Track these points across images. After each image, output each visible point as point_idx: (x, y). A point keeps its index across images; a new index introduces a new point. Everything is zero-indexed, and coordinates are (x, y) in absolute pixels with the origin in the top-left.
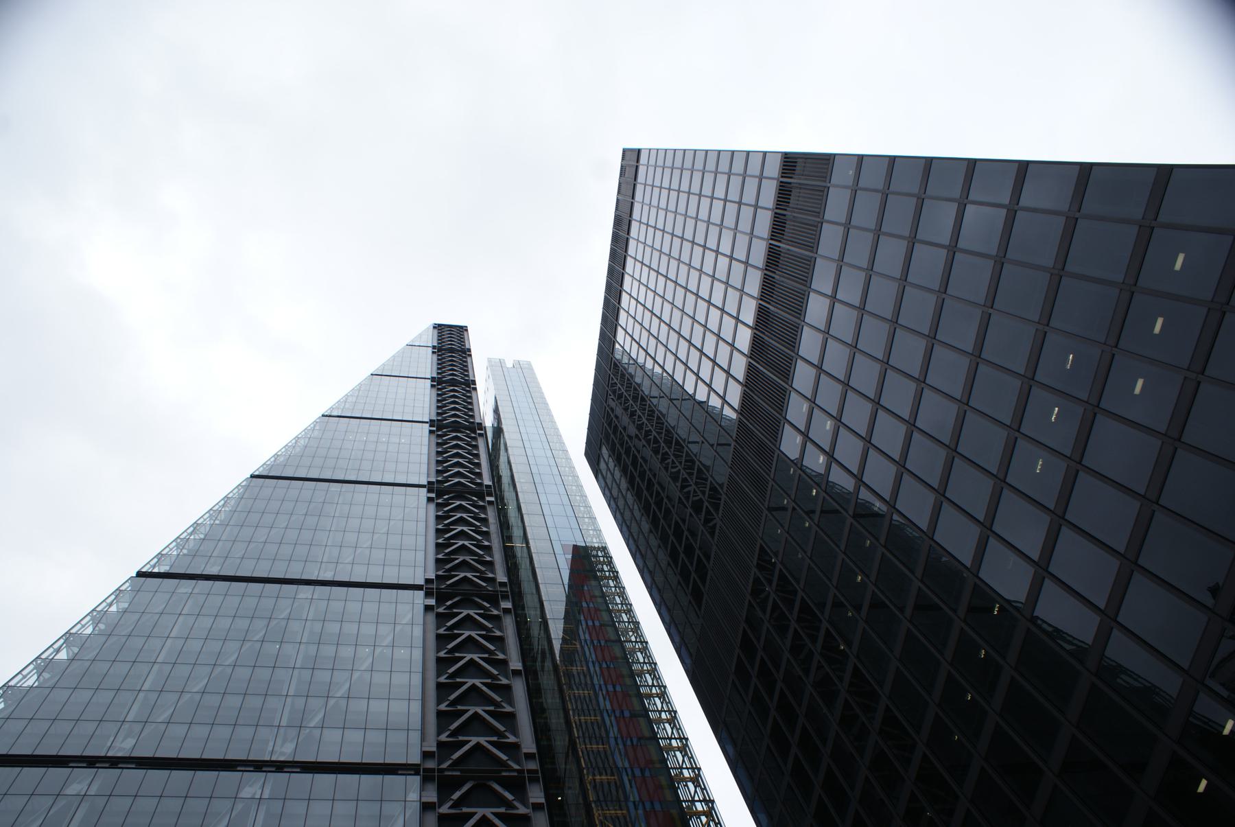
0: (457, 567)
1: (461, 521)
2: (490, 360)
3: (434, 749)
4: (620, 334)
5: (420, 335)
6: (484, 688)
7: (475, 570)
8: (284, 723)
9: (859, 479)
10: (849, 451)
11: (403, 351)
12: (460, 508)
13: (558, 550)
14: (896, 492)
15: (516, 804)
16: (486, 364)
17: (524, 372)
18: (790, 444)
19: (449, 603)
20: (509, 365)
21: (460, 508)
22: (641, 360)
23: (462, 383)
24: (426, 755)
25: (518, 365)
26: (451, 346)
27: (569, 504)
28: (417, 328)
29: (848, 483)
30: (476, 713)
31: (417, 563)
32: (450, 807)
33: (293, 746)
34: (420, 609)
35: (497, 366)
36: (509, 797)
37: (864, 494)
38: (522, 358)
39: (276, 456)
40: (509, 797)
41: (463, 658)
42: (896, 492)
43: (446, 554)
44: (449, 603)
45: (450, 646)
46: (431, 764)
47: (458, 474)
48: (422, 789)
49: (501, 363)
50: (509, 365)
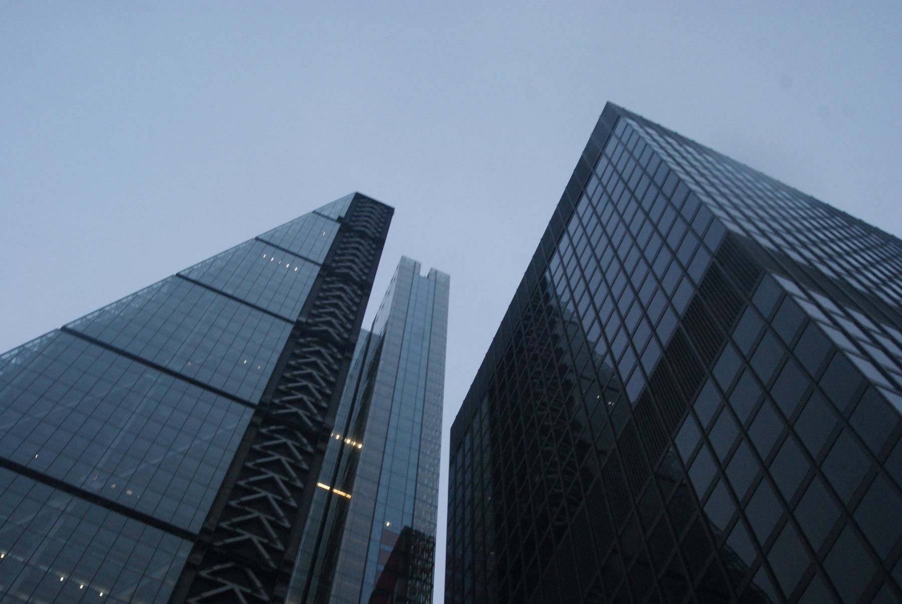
0: (243, 525)
1: (305, 389)
2: (404, 260)
3: (213, 529)
4: (565, 242)
5: (335, 204)
6: (260, 547)
7: (290, 454)
8: (113, 446)
9: (763, 553)
10: (765, 512)
11: (305, 219)
12: (318, 354)
13: (376, 535)
14: (773, 538)
15: (262, 591)
16: (397, 262)
17: (438, 286)
18: (686, 438)
19: (217, 568)
20: (424, 272)
21: (318, 354)
22: (586, 324)
23: (355, 282)
24: (204, 530)
25: (434, 273)
26: (363, 225)
27: (414, 474)
28: (332, 192)
29: (747, 554)
30: (250, 540)
31: (293, 309)
32: (209, 574)
33: (101, 486)
34: (180, 564)
35: (409, 269)
36: (259, 584)
37: (761, 580)
38: (442, 268)
39: (102, 311)
40: (259, 584)
41: (224, 585)
42: (773, 538)
43: (282, 401)
44: (217, 568)
45: (244, 499)
46: (207, 539)
47: (329, 323)
48: (193, 551)
49: (416, 266)
50: (424, 272)
